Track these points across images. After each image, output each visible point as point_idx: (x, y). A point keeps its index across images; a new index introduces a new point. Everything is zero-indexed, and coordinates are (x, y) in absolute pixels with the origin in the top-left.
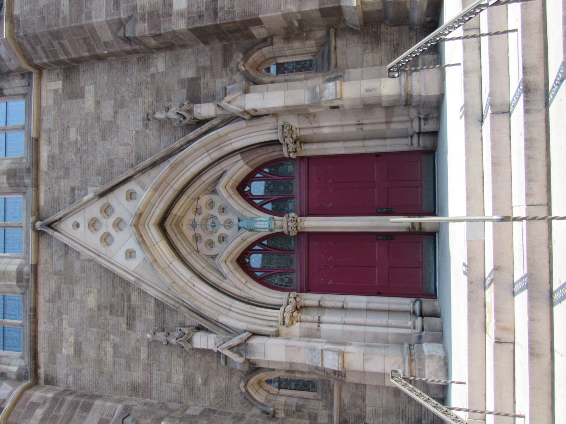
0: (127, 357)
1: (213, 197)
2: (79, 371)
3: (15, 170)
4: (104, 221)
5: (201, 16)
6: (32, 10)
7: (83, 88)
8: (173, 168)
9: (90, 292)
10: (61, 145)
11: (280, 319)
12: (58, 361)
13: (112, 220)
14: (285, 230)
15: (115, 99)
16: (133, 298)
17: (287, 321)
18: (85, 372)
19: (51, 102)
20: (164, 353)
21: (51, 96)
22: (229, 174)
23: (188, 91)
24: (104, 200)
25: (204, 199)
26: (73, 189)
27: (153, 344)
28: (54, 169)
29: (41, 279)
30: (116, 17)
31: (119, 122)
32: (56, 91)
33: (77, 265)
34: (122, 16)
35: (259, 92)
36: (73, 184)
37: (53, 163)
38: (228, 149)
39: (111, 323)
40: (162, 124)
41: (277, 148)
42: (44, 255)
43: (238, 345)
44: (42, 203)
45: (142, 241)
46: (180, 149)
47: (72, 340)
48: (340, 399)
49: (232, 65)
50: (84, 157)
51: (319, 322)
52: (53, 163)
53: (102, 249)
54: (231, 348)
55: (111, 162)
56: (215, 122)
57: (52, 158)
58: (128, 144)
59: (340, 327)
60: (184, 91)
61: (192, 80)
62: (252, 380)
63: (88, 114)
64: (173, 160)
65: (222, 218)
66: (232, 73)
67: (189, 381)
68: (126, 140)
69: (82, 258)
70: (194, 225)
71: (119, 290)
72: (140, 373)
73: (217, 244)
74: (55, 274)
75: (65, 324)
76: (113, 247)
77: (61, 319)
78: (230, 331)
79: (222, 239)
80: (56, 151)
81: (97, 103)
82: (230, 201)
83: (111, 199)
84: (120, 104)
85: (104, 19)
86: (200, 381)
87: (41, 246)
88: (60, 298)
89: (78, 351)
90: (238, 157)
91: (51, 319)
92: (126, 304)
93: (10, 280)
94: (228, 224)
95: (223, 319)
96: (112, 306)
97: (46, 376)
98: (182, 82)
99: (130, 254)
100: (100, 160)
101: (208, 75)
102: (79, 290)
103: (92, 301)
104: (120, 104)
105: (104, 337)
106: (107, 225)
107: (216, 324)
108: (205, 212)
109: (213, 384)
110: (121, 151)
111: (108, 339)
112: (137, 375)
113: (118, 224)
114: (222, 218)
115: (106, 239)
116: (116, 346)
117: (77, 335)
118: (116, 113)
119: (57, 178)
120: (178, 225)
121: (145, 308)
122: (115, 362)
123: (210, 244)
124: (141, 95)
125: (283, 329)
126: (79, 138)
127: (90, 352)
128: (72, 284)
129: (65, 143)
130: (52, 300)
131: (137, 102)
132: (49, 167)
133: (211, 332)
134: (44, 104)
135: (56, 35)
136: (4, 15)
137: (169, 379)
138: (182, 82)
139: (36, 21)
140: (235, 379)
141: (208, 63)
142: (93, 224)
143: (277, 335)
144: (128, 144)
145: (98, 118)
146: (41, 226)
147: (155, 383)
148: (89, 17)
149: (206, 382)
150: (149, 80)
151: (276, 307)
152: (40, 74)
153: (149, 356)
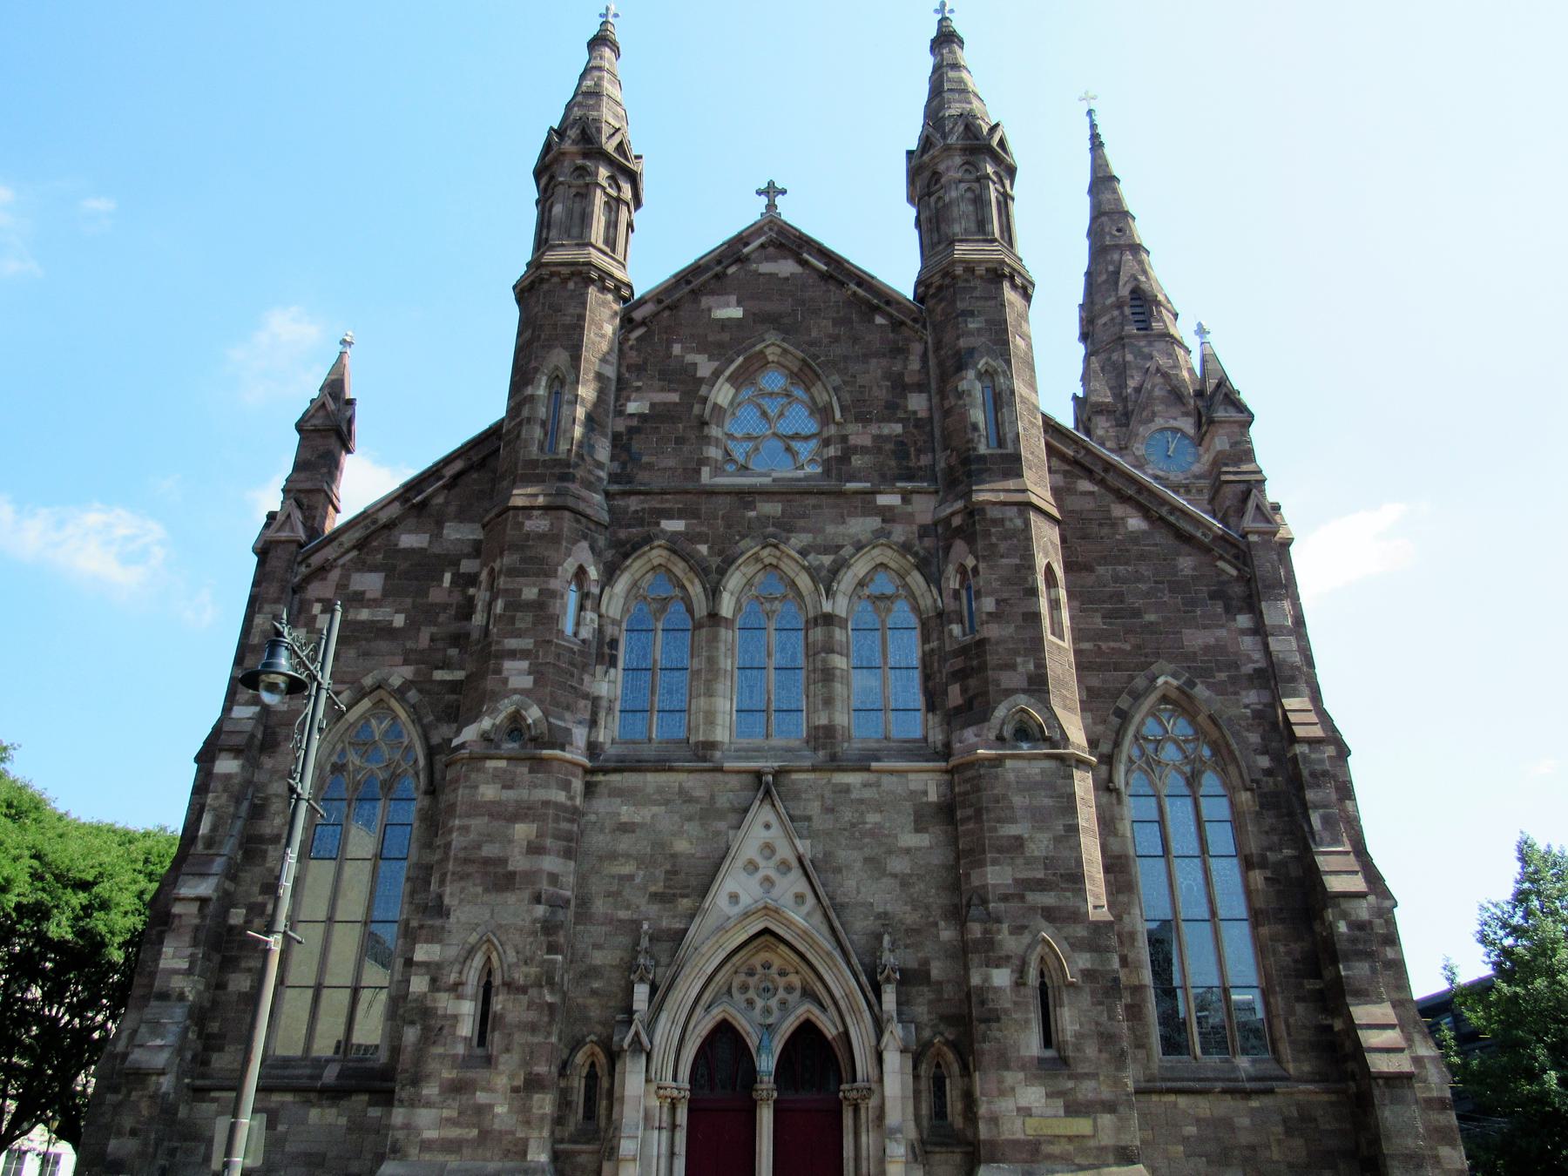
0: (618, 894)
1: (797, 993)
2: (602, 830)
3: (834, 737)
4: (772, 863)
5: (983, 1003)
6: (1008, 785)
7: (927, 832)
8: (829, 954)
9: (692, 843)
10: (861, 801)
11: (664, 1084)
12: (613, 800)
13: (772, 873)
14: (758, 1086)
15: (910, 876)
16: (685, 900)
17: (662, 1092)
18: (601, 837)
19: (912, 787)
20: (625, 940)
21: (920, 787)
22: (823, 1017)
23: (915, 970)
24: (794, 863)
25: (795, 980)
26: (809, 819)
27: (637, 924)
28: (834, 792)
29: (707, 777)
30: (990, 897)
31: (884, 880)
32: (925, 793)
33: (721, 825)
34: (991, 905)
35: (902, 1067)
36: (815, 818)
37: (840, 792)
38: (848, 1020)
39: (657, 872)
40: (879, 937)
41: (850, 1078)
42: (734, 781)
43: (640, 1043)
44: (794, 776)
45: (746, 915)
46: (849, 963)
47: (638, 819)
48: (580, 1153)
49: (942, 1027)
50: (846, 833)
51: (660, 1128)
52: (840, 792)
53: (740, 863)
54: (637, 1034)
55: (838, 870)
56: (876, 1008)
57: (847, 789)
58: (858, 893)
59: (655, 1153)
60: (916, 966)
61: (928, 973)
62: (597, 1049)
63: (896, 836)
64: (837, 954)
65: (774, 1003)
66: (932, 1027)
67: (593, 972)
68: (863, 890)
69: (731, 833)
70: (767, 966)
71: (693, 882)
72: (601, 910)
73: (744, 997)
74: (712, 797)
75: (655, 809)
76: (743, 876)
77: (660, 805)
78: (651, 1026)
79: (750, 1003)
80: (854, 795)
81: (908, 851)
82: (792, 1018)
83: (796, 873)
84: (904, 882)
85: (990, 881)
86: (596, 985)
87: (744, 776)
88: (685, 802)
89: (626, 828)
90: (841, 1029)
91: (660, 790)
92: (678, 892)
93: (704, 731)
94: (767, 1011)
95: (664, 1017)
96: (675, 873)
97: (596, 784)
98: (925, 963)
99: (734, 898)
100: (842, 855)
101: (932, 996)
102: (693, 828)
103: (681, 846)
104: (904, 882)
105: (641, 861)
106: (767, 869)
107: (660, 1008)
108: (781, 982)
109: (592, 1001)
110: (851, 884)
111: (638, 868)
112: (600, 906)
113: (768, 881)
114: (774, 1003)
115: (752, 867)
116: (631, 877)
117: (642, 825)
118: (895, 876)
119: (823, 797)
120: (767, 948)
121: (674, 917)
122: (613, 877)
123: (744, 988)
124: (915, 909)
125: (653, 1087)
126: (868, 826)
127: (625, 843)
128: (701, 818)
129: (863, 807)
130: (682, 791)
131: (906, 904)
132: (835, 785)
133: (650, 1002)
134: (911, 776)
135: (978, 815)
136: (1005, 749)
137: (597, 946)
138: (925, 963)
139: (996, 792)
140: (599, 1028)
141: (946, 996)
142: (768, 849)
143: (648, 1081)
144: (858, 893)
145: (890, 852)
146: (767, 783)
147: (592, 929)
148: (995, 862)
149: (594, 993)
150: (931, 919)
151: (675, 1079)
152: (947, 771)
153: (620, 921)
